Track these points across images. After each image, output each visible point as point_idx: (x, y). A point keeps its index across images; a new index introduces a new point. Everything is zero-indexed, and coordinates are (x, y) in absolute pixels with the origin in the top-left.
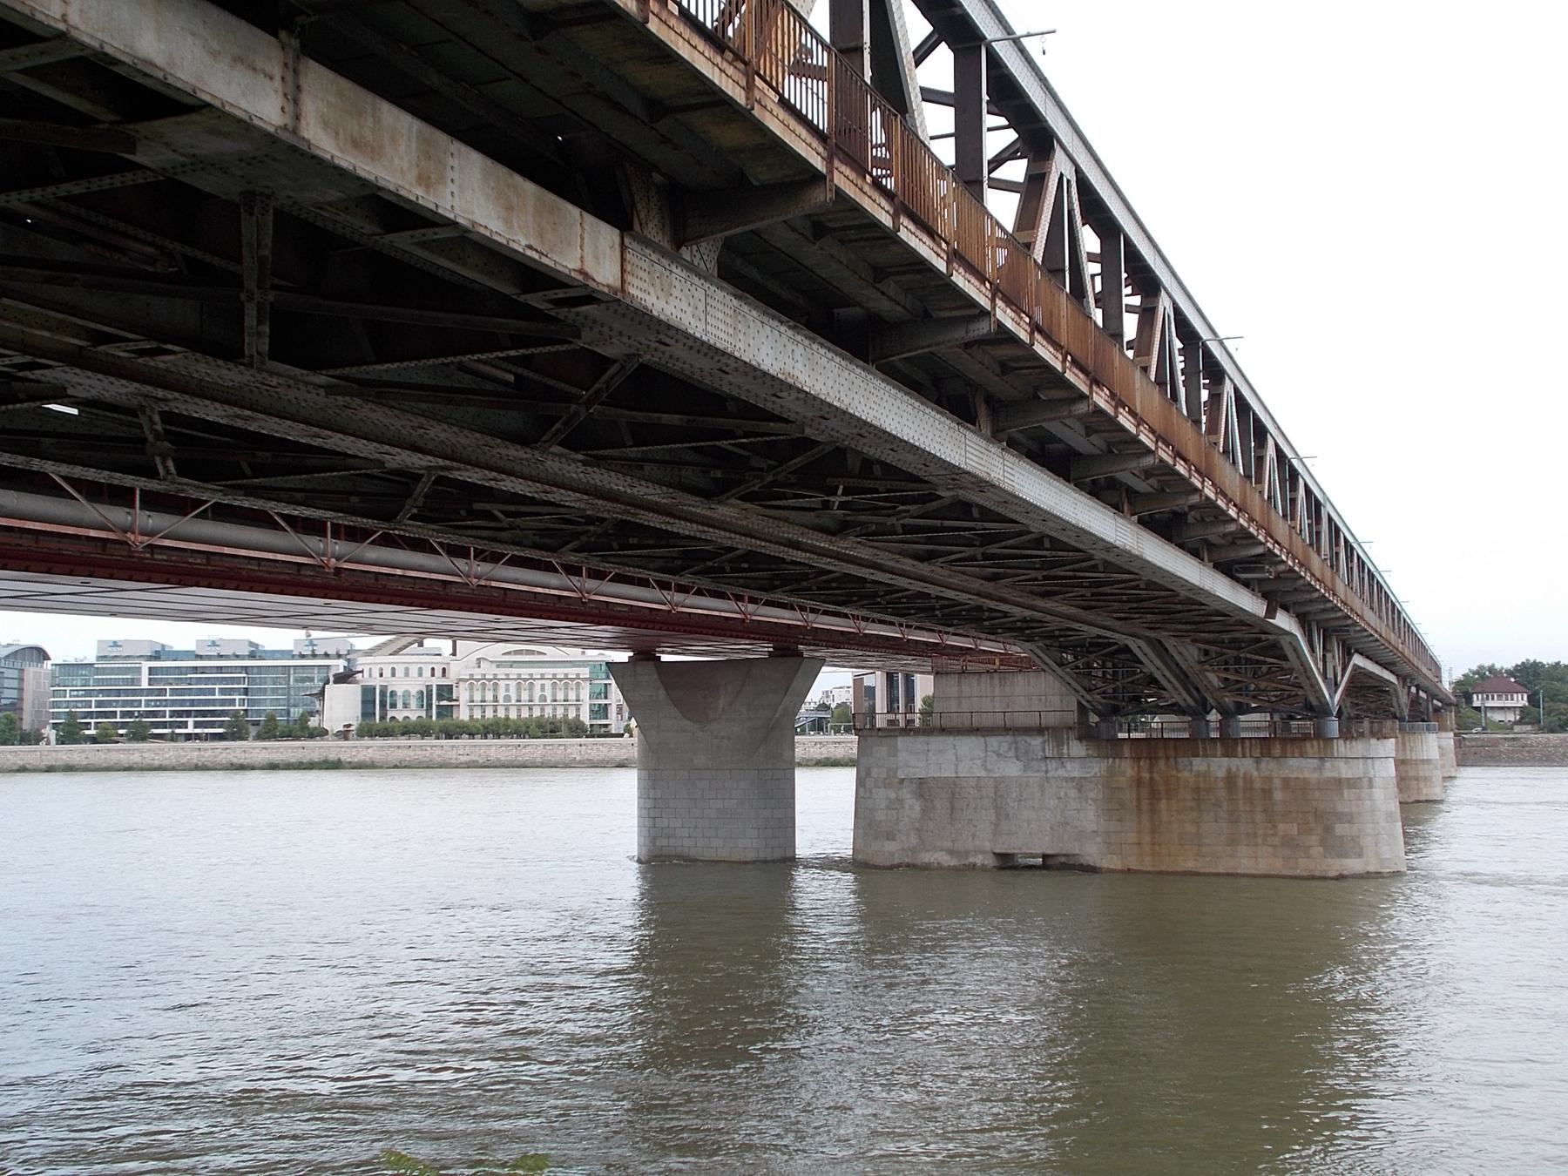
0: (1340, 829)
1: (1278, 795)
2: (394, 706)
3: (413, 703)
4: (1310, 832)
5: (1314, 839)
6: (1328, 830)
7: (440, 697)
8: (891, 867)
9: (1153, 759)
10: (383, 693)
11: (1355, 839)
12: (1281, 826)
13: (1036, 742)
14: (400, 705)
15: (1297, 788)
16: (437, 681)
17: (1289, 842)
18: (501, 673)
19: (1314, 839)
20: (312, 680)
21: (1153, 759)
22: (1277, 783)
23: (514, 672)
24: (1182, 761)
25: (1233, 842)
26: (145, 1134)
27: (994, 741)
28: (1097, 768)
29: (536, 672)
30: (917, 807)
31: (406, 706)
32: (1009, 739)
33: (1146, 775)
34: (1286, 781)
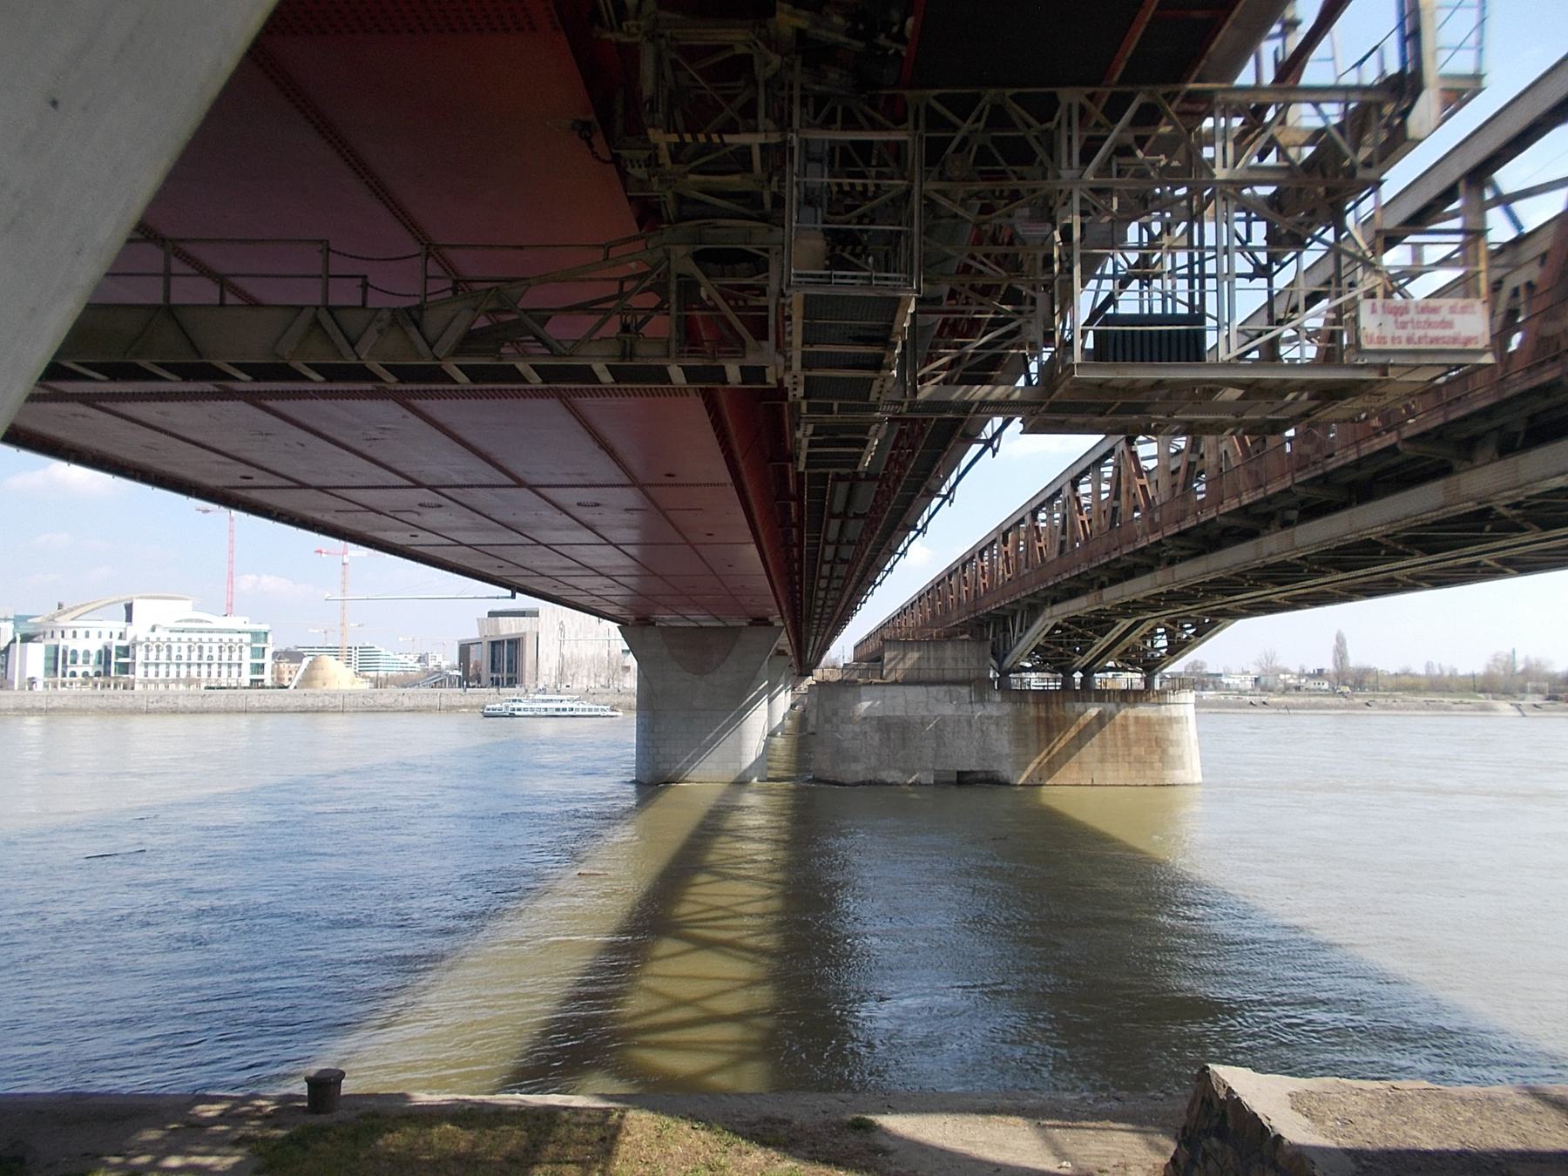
0: (1171, 751)
1: (1132, 729)
2: (74, 662)
3: (93, 659)
4: (1152, 753)
5: (1156, 757)
6: (1164, 752)
7: (118, 656)
8: (857, 784)
9: (1048, 704)
10: (65, 652)
11: (1180, 757)
12: (1134, 750)
13: (965, 690)
14: (80, 661)
15: (1146, 724)
16: (117, 642)
17: (1140, 760)
18: (174, 636)
19: (1156, 757)
20: (1143, 487)
21: (1048, 704)
22: (1131, 721)
23: (185, 637)
24: (1068, 705)
25: (1102, 760)
26: (198, 972)
27: (933, 690)
28: (1007, 708)
29: (205, 637)
30: (877, 738)
31: (86, 662)
32: (945, 688)
33: (1043, 714)
34: (1137, 718)
